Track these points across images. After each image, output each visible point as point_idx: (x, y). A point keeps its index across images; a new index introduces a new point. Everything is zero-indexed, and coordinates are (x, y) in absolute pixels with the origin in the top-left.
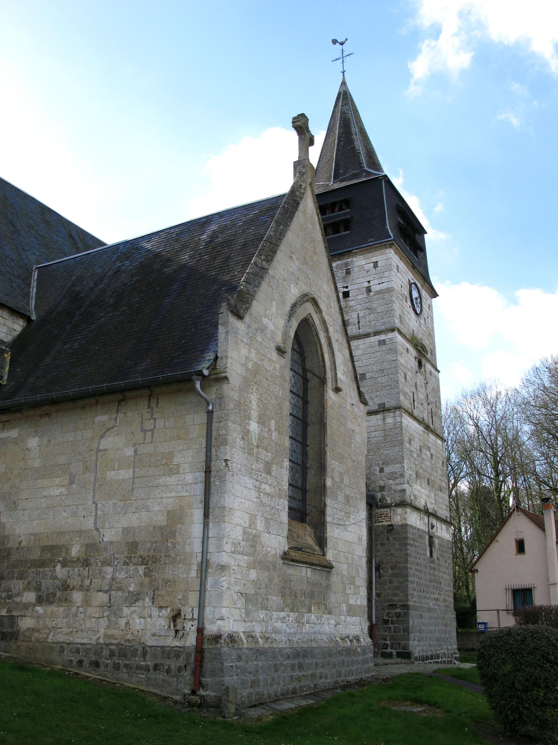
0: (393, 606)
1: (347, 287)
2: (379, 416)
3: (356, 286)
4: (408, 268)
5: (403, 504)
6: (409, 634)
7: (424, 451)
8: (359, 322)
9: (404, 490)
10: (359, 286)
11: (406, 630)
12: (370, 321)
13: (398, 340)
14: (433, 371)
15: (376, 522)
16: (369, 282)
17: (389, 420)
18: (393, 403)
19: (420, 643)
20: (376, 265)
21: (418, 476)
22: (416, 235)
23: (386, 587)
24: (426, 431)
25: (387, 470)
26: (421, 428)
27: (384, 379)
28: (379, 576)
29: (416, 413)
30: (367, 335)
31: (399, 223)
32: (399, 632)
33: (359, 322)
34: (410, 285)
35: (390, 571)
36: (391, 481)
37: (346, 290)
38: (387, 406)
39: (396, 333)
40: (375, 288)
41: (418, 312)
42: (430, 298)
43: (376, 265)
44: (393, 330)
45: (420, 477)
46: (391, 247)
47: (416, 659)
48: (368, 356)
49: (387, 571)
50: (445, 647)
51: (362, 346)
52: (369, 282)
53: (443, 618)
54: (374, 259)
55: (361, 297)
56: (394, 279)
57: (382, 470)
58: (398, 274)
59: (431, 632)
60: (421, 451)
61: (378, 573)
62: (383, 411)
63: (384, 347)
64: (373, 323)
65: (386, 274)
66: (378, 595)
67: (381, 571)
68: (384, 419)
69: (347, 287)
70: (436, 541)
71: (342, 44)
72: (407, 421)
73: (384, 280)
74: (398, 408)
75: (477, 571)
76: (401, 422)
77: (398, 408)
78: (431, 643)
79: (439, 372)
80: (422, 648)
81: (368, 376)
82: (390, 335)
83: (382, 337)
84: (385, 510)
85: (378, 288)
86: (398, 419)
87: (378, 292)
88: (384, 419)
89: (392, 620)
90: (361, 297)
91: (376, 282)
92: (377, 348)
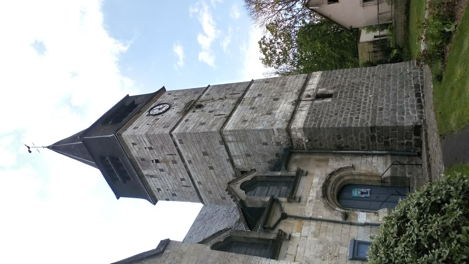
0: (373, 138)
1: (153, 161)
2: (229, 145)
3: (150, 155)
4: (139, 116)
5: (288, 130)
6: (397, 126)
7: (254, 104)
8: (172, 155)
9: (278, 129)
10: (149, 153)
11: (394, 128)
12: (169, 148)
13: (178, 131)
14: (209, 88)
15: (304, 149)
16: (146, 148)
17: (230, 138)
18: (219, 135)
19: (405, 110)
20: (134, 144)
21: (269, 113)
22: (126, 105)
23: (356, 142)
24: (241, 102)
25: (265, 140)
26: (239, 107)
27: (204, 141)
28: (347, 148)
29: (227, 113)
30: (178, 150)
31: (112, 123)
32: (396, 133)
33: (172, 155)
34: (149, 115)
35: (342, 139)
36: (272, 138)
37: (154, 161)
38: (221, 140)
39: (173, 133)
40: (149, 145)
41: (168, 106)
42: (166, 92)
43: (134, 144)
44: (171, 136)
45: (270, 111)
46: (121, 135)
47: (421, 118)
48: (191, 150)
49: (342, 141)
50: (408, 76)
51: (186, 153)
52: (146, 148)
53: (383, 80)
54: (131, 145)
55: (156, 153)
56: (140, 133)
57: (266, 144)
58: (139, 127)
59: (395, 95)
60: (253, 108)
61: (345, 148)
62: (225, 142)
63: (183, 141)
64: (170, 146)
65: (138, 138)
66: (363, 148)
67: (343, 145)
68: (230, 142)
69: (153, 161)
70: (321, 90)
71: (29, 148)
72: (229, 126)
73: (142, 139)
74: (221, 132)
75: (351, 27)
76: (230, 131)
77: (221, 132)
78: (405, 94)
79: (209, 86)
80: (409, 108)
81: (204, 151)
82: (175, 136)
83: (177, 142)
84: (294, 142)
85: (148, 143)
86: (228, 133)
87: (151, 143)
88: (230, 142)
89: (385, 139)
90: (156, 153)
91: (145, 144)
92: (185, 145)
